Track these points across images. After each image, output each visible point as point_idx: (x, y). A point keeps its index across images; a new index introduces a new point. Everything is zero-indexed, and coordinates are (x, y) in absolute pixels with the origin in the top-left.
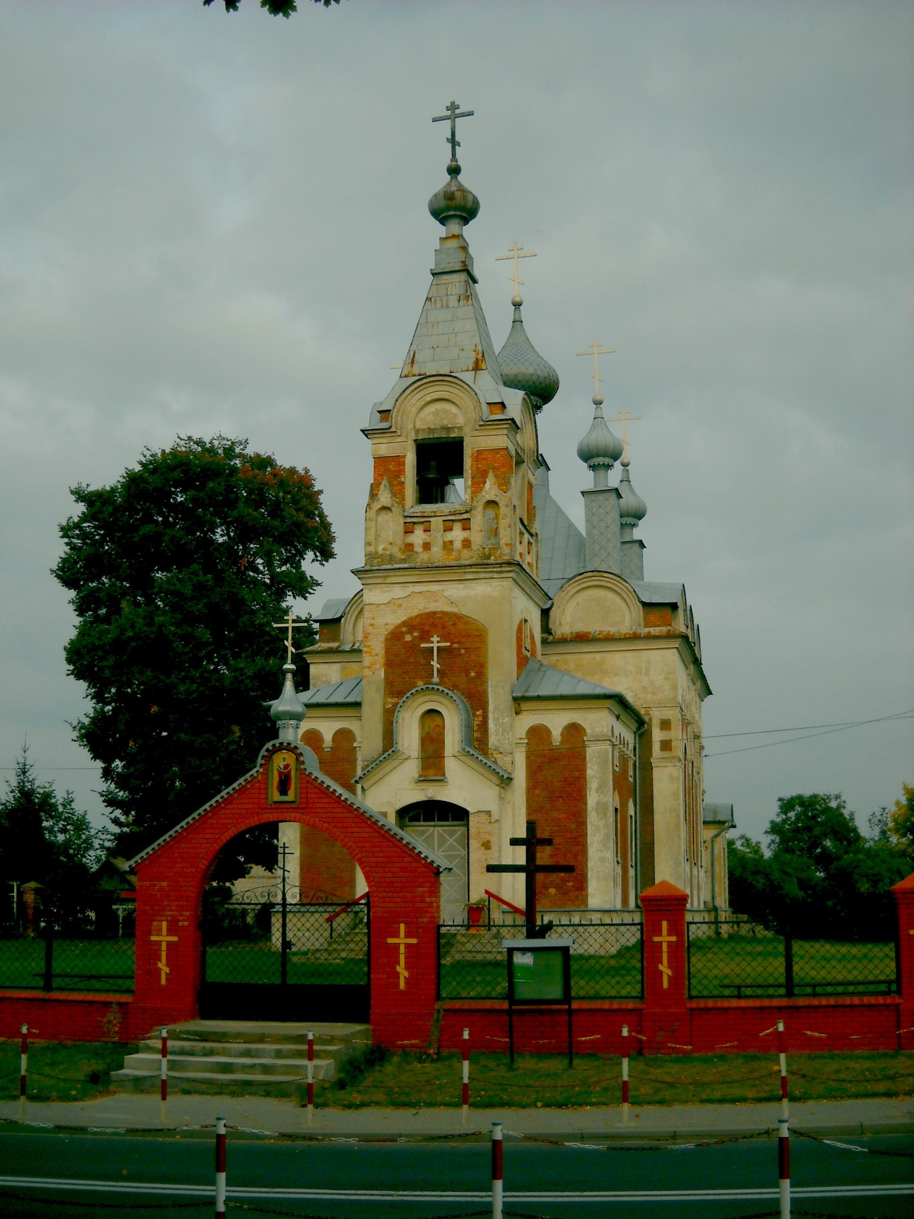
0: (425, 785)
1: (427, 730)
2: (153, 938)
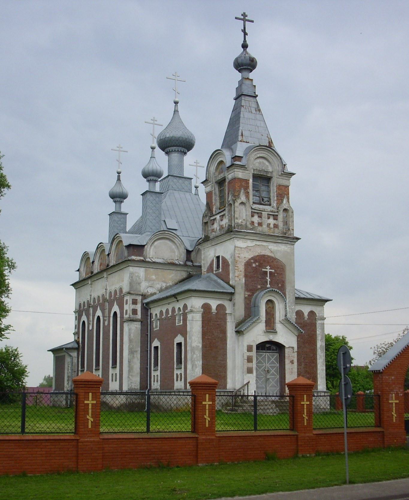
0: (269, 334)
2: (390, 402)
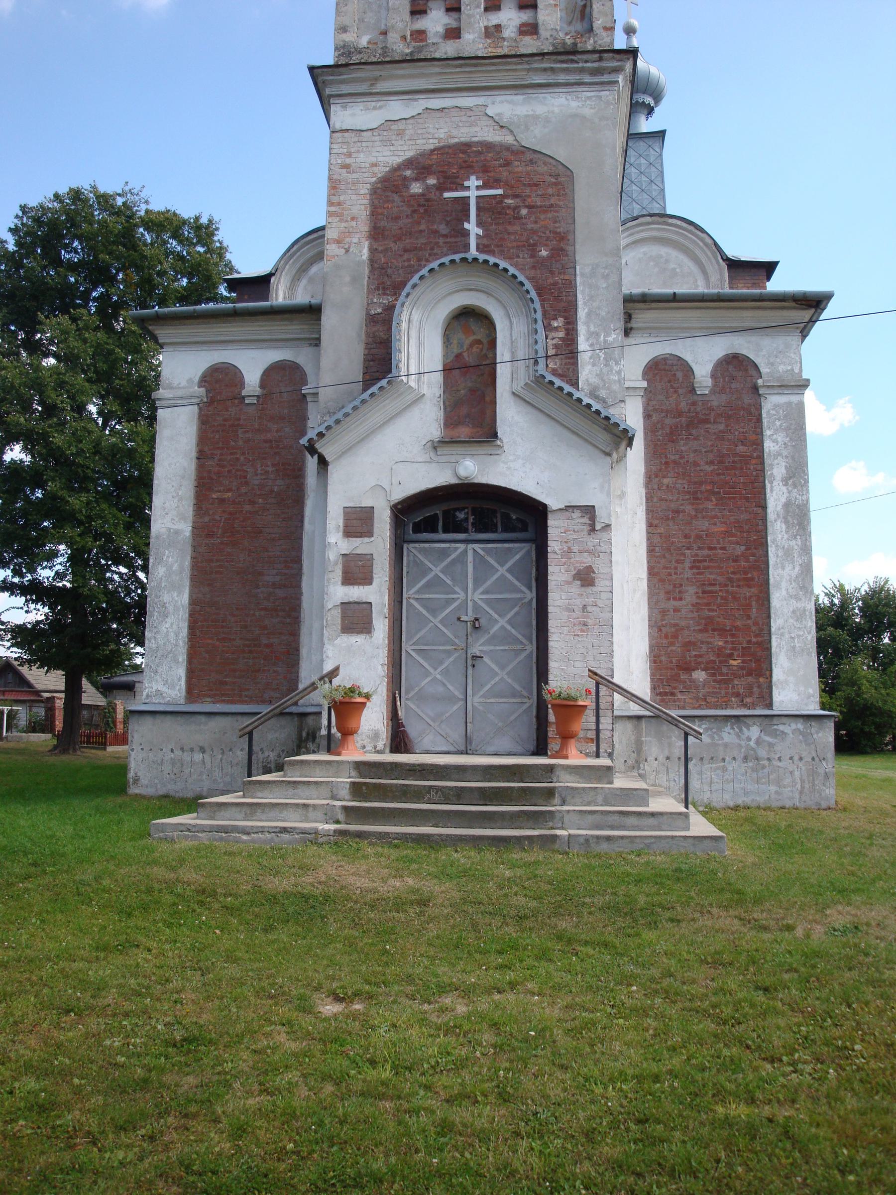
1: (456, 351)
